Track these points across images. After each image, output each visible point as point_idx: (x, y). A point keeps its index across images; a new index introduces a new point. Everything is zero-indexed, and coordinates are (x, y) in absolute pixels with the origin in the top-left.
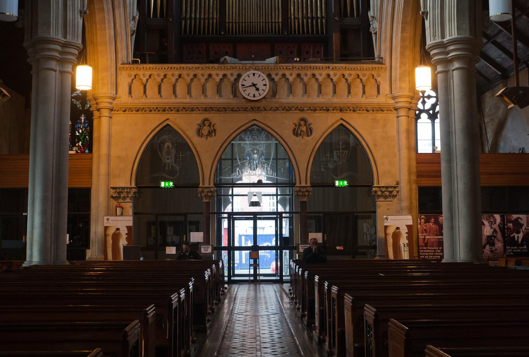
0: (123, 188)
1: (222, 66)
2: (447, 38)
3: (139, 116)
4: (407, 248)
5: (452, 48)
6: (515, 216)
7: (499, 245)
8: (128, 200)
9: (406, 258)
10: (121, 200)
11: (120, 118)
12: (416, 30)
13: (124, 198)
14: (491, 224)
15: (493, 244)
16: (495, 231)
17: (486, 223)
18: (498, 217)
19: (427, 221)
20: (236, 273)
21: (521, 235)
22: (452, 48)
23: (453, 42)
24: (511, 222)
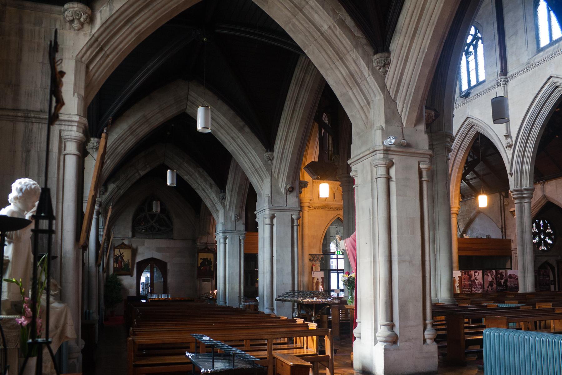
0: (316, 255)
1: (460, 181)
2: (524, 188)
3: (322, 212)
4: (458, 288)
5: (525, 192)
6: (501, 271)
7: (495, 286)
8: (318, 262)
9: (44, 228)
10: (314, 262)
11: (314, 212)
12: (433, 191)
13: (316, 261)
14: (492, 275)
15: (492, 286)
16: (493, 279)
17: (489, 274)
18: (494, 271)
19: (465, 274)
20: (47, 228)
21: (503, 281)
22: (525, 192)
23: (526, 190)
24: (499, 274)
